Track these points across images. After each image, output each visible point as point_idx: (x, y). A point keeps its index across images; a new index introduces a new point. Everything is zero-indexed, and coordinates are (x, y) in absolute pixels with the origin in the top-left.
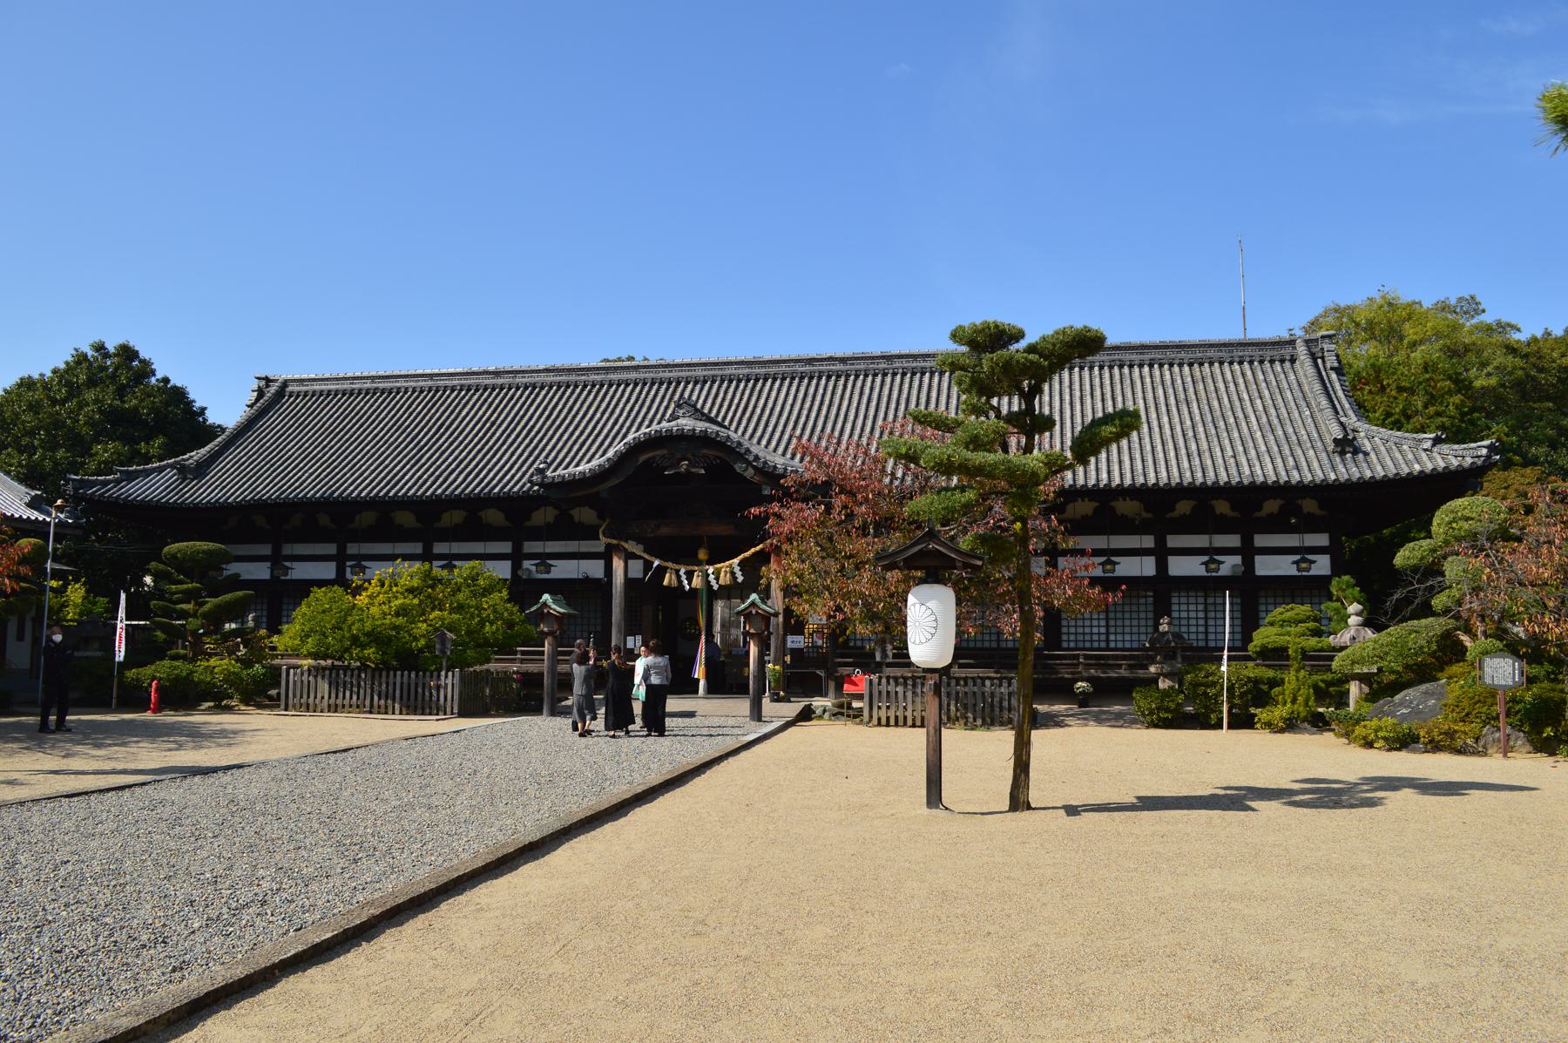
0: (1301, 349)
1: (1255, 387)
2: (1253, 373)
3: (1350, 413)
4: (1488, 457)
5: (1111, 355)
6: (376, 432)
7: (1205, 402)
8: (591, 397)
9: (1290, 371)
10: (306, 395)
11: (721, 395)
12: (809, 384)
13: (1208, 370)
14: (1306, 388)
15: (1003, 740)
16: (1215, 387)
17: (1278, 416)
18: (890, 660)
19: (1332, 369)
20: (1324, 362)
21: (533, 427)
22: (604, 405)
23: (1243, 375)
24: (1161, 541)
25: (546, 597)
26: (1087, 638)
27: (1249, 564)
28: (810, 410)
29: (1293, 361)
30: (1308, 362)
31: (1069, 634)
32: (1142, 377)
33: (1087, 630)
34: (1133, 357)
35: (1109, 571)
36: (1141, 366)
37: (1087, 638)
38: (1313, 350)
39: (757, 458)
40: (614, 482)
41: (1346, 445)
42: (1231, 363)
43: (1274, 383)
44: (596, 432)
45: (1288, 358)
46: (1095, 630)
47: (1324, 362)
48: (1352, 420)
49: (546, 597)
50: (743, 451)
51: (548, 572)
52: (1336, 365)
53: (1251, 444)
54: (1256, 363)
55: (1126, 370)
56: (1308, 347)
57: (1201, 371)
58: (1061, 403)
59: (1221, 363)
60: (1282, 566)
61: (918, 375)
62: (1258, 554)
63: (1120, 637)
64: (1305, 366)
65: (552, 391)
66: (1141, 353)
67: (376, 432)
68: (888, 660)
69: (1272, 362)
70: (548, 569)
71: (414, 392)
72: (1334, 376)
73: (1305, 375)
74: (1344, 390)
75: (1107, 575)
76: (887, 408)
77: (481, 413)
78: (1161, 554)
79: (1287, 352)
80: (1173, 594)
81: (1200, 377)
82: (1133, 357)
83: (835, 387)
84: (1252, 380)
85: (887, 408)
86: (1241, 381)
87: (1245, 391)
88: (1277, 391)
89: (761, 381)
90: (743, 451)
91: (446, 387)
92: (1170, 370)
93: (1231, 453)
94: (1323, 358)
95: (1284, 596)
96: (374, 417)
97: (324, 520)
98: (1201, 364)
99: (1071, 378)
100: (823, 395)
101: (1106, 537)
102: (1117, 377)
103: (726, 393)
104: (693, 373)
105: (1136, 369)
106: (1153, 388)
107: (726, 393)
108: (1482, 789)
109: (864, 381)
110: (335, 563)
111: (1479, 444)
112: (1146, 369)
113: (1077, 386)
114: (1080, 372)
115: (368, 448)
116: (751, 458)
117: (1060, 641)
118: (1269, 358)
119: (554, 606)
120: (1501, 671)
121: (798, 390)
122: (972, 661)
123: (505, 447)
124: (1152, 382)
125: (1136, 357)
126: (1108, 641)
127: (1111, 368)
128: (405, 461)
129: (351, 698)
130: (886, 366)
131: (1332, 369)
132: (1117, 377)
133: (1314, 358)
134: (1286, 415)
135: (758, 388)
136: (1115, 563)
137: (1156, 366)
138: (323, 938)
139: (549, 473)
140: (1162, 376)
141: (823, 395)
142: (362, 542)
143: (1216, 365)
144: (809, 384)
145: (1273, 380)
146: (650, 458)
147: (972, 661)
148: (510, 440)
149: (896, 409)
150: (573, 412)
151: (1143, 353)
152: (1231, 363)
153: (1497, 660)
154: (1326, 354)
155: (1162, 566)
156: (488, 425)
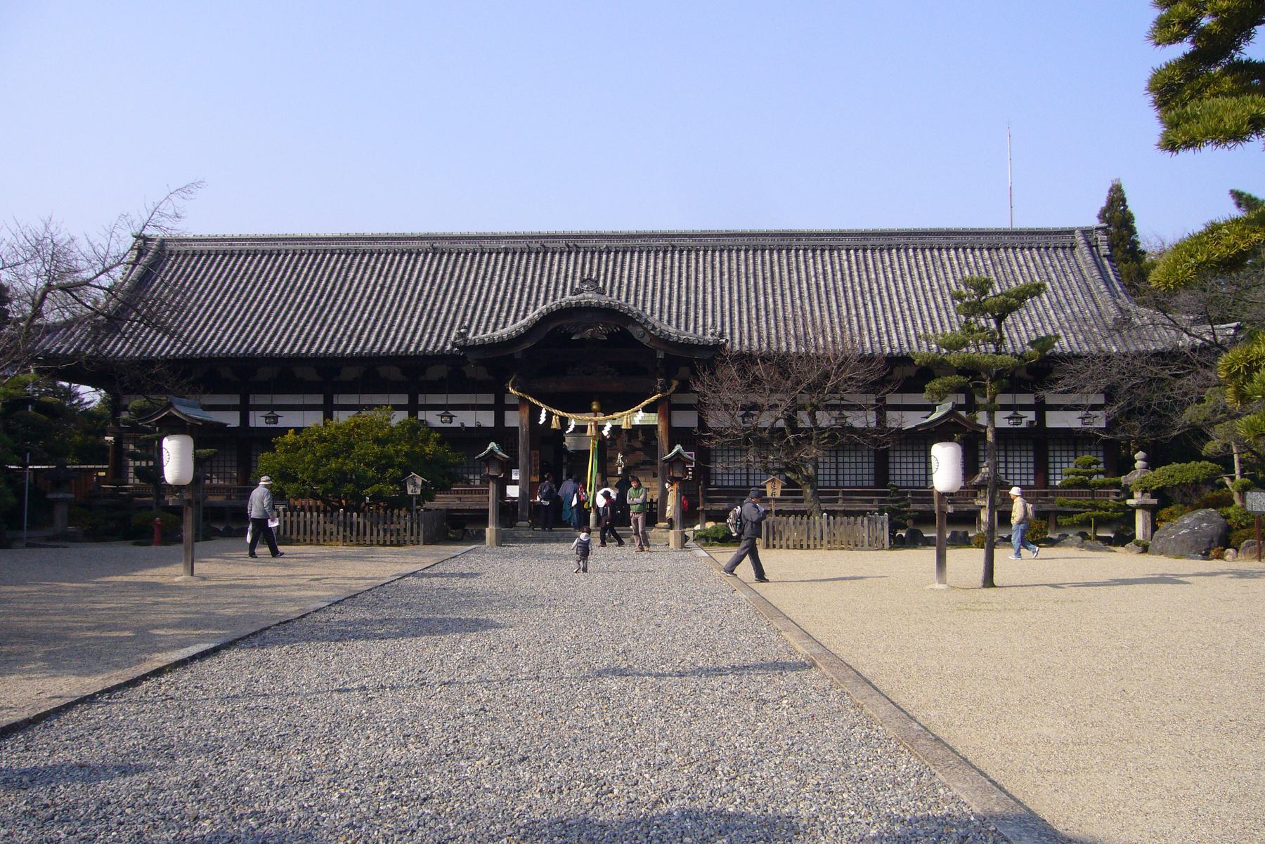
0: (1079, 239)
1: (1043, 270)
2: (1041, 258)
3: (1122, 295)
4: (1234, 335)
5: (922, 239)
6: (271, 292)
7: (1005, 283)
8: (468, 263)
9: (1071, 257)
10: (186, 255)
11: (588, 265)
12: (664, 258)
13: (1004, 255)
14: (1085, 272)
15: (980, 554)
16: (1011, 269)
17: (1065, 297)
18: (778, 496)
19: (1104, 256)
20: (1097, 249)
21: (422, 291)
22: (482, 272)
23: (1033, 260)
24: (328, 400)
25: (492, 445)
26: (904, 478)
27: (1041, 418)
28: (671, 281)
29: (1072, 248)
30: (1086, 251)
31: (1021, 474)
32: (950, 259)
33: (910, 472)
34: (941, 241)
35: (446, 422)
36: (948, 249)
37: (910, 478)
38: (1090, 239)
39: (654, 328)
40: (528, 345)
41: (1123, 323)
42: (1022, 249)
43: (1059, 268)
44: (483, 297)
45: (1069, 245)
46: (917, 472)
47: (1097, 249)
48: (1124, 301)
49: (492, 445)
50: (643, 321)
51: (276, 422)
52: (1108, 253)
53: (1047, 321)
54: (1042, 250)
55: (936, 253)
56: (1084, 236)
57: (998, 255)
58: (886, 280)
59: (1014, 248)
60: (1070, 420)
61: (759, 252)
62: (241, 415)
63: (917, 478)
64: (1083, 255)
65: (218, 259)
66: (947, 238)
67: (271, 292)
68: (776, 497)
69: (1055, 248)
70: (276, 419)
71: (294, 254)
72: (1106, 262)
73: (1085, 262)
74: (1115, 274)
75: (268, 426)
76: (739, 281)
77: (367, 276)
78: (244, 410)
79: (1067, 240)
80: (980, 442)
81: (997, 260)
82: (941, 241)
83: (688, 260)
84: (1041, 265)
85: (739, 281)
86: (1031, 265)
87: (1036, 274)
88: (1062, 274)
89: (360, 256)
90: (643, 321)
91: (325, 250)
92: (972, 253)
93: (1031, 328)
94: (1096, 246)
95: (1060, 445)
96: (263, 278)
97: (471, 371)
98: (997, 249)
99: (890, 258)
100: (680, 268)
101: (445, 395)
102: (929, 258)
103: (591, 263)
104: (276, 246)
105: (944, 252)
106: (961, 270)
107: (591, 263)
108: (1144, 583)
109: (713, 256)
110: (1047, 412)
111: (1228, 325)
112: (952, 252)
113: (896, 265)
114: (872, 254)
115: (270, 308)
116: (650, 327)
117: (888, 481)
118: (1053, 246)
119: (500, 453)
120: (1258, 501)
121: (655, 263)
122: (726, 497)
123: (394, 310)
124: (959, 264)
125: (943, 242)
126: (837, 480)
127: (747, 251)
128: (312, 321)
129: (378, 534)
130: (730, 243)
131: (1104, 256)
132: (929, 258)
133: (1090, 247)
134: (1071, 296)
135: (428, 260)
136: (451, 417)
137: (960, 250)
138: (39, 712)
139: (470, 336)
140: (966, 258)
141: (680, 268)
142: (275, 393)
143: (1010, 250)
144: (664, 258)
145: (1058, 264)
146: (558, 327)
147: (726, 497)
148: (404, 304)
149: (747, 282)
150: (455, 278)
151: (949, 238)
152: (1022, 249)
153: (1255, 494)
154: (1099, 243)
155: (881, 420)
156: (378, 288)
